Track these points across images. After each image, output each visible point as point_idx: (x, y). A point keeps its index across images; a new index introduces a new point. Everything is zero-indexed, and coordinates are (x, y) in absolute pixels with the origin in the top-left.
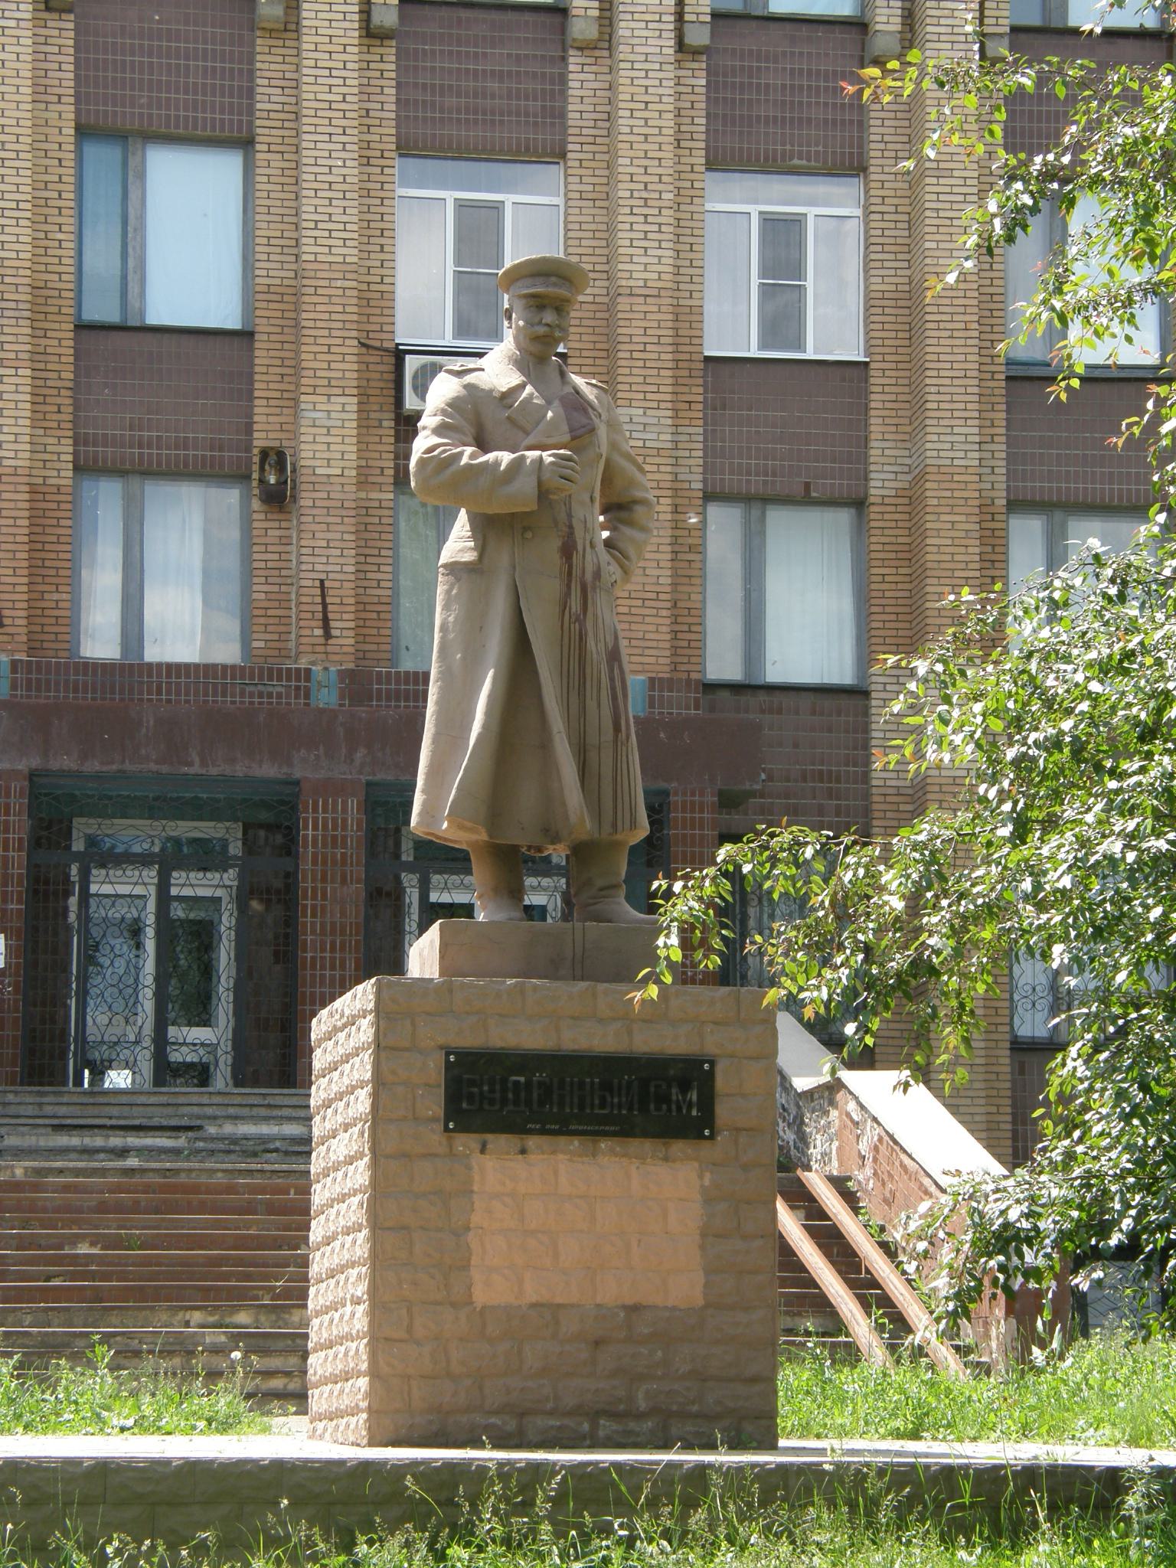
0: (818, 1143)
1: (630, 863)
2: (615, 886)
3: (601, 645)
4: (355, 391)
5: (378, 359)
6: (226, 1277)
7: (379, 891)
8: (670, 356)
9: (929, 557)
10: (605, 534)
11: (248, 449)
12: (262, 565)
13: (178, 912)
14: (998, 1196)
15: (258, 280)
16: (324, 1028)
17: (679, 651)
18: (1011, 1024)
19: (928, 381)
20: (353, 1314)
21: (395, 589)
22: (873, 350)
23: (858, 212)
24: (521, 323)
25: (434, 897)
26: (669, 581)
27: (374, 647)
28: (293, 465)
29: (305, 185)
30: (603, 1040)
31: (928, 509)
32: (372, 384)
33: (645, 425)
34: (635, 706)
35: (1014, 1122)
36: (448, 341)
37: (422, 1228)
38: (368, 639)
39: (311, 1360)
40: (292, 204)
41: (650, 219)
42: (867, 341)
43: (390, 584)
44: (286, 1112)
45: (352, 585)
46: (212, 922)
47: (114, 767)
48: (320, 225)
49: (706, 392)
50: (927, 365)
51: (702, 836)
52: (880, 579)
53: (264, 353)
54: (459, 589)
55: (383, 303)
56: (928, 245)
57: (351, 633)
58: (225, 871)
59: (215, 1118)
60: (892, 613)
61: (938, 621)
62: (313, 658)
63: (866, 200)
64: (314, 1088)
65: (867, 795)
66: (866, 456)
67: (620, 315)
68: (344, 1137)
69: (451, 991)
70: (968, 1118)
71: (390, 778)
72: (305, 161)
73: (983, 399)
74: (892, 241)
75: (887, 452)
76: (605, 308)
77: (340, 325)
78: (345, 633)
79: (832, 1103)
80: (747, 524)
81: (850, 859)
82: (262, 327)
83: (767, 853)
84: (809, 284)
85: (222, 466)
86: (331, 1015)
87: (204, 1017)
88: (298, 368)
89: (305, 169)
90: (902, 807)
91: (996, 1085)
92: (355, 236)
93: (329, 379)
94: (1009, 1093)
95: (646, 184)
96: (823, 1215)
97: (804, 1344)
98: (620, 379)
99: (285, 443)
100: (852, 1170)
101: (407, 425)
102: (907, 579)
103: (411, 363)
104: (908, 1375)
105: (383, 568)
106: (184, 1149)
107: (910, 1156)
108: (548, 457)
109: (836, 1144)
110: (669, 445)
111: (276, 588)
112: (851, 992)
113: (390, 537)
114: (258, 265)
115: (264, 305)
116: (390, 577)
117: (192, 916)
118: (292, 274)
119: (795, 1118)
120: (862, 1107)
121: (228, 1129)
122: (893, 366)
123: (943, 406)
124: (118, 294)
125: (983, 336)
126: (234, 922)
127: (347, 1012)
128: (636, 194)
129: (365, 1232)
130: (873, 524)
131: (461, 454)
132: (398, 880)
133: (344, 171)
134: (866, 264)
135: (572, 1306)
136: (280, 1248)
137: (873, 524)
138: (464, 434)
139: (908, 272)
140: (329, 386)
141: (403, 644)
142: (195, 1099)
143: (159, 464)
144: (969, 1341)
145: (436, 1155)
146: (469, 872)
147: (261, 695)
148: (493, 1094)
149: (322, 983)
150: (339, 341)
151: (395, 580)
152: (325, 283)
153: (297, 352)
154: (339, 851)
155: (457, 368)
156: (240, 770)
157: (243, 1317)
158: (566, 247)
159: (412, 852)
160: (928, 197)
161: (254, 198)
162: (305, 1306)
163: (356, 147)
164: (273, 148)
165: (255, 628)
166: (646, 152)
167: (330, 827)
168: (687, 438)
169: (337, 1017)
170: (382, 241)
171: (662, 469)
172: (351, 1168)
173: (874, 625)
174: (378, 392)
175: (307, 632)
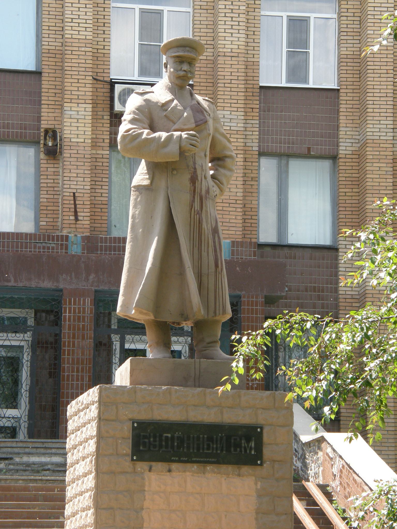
0: (313, 468)
2: (215, 342)
5: (102, 86)
7: (100, 343)
10: (212, 172)
11: (39, 129)
15: (44, 47)
16: (73, 410)
17: (246, 228)
22: (342, 83)
23: (335, 16)
24: (172, 70)
25: (127, 346)
26: (242, 194)
27: (99, 225)
28: (61, 137)
31: (368, 161)
32: (99, 98)
33: (231, 119)
34: (225, 255)
36: (136, 78)
38: (96, 221)
40: (61, 10)
41: (234, 19)
42: (338, 79)
43: (107, 195)
44: (53, 451)
45: (89, 195)
46: (19, 358)
48: (74, 21)
49: (260, 103)
50: (368, 91)
51: (257, 318)
54: (141, 197)
57: (88, 218)
58: (26, 333)
59: (19, 454)
60: (349, 210)
62: (69, 230)
63: (339, 10)
64: (68, 439)
65: (336, 299)
66: (338, 135)
67: (219, 66)
68: (82, 463)
69: (170, 393)
71: (106, 288)
74: (352, 30)
75: (348, 133)
78: (85, 218)
79: (320, 448)
82: (45, 70)
83: (288, 325)
84: (311, 51)
85: (25, 137)
86: (77, 403)
87: (14, 404)
88: (63, 90)
90: (354, 305)
92: (91, 26)
93: (78, 95)
96: (315, 503)
99: (56, 126)
100: (329, 482)
101: (116, 118)
102: (357, 194)
103: (118, 88)
106: (3, 469)
107: (358, 475)
108: (184, 135)
109: (321, 469)
111: (52, 197)
113: (107, 172)
116: (107, 191)
117: (9, 355)
119: (302, 455)
120: (334, 450)
121: (25, 459)
123: (375, 110)
126: (29, 358)
129: (92, 510)
130: (341, 168)
131: (142, 133)
132: (110, 338)
134: (338, 42)
136: (50, 518)
138: (144, 123)
140: (78, 99)
141: (113, 223)
142: (9, 445)
145: (127, 473)
147: (44, 248)
148: (155, 442)
149: (72, 388)
151: (110, 193)
153: (63, 82)
154: (81, 324)
155: (141, 91)
156: (33, 284)
158: (194, 32)
161: (42, 7)
165: (42, 216)
167: (77, 311)
168: (251, 125)
169: (80, 404)
170: (104, 28)
172: (86, 479)
173: (341, 216)
174: (102, 102)
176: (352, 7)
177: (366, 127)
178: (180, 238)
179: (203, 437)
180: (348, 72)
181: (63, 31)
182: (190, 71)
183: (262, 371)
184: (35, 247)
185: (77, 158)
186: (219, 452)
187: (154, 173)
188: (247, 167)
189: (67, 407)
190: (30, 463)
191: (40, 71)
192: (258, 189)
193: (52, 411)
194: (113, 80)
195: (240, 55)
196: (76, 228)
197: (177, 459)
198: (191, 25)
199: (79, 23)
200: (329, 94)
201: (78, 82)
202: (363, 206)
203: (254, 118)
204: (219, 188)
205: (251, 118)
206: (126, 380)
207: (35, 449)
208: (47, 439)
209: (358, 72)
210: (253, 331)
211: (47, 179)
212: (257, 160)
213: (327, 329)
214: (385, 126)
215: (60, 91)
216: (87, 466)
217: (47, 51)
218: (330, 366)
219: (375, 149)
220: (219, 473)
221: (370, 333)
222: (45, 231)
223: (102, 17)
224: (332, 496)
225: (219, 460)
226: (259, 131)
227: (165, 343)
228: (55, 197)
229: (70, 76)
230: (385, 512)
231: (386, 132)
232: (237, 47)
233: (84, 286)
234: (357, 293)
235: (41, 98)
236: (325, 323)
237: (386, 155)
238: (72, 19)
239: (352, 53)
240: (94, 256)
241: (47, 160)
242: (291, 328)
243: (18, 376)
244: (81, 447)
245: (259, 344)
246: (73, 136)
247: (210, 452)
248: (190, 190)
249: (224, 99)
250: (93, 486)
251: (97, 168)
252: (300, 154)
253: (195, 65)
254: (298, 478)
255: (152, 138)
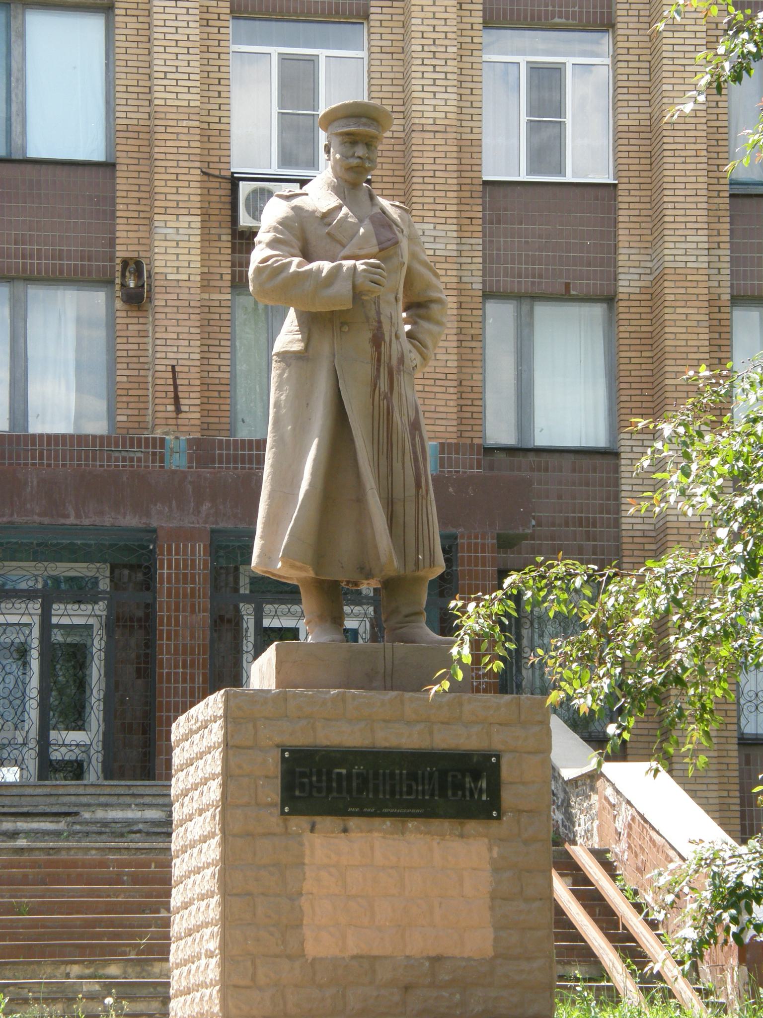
0: (582, 822)
1: (429, 594)
2: (418, 614)
3: (405, 418)
4: (199, 212)
5: (217, 185)
6: (99, 936)
7: (221, 618)
8: (455, 181)
9: (667, 343)
10: (407, 328)
11: (112, 259)
12: (125, 354)
13: (58, 637)
14: (733, 860)
15: (119, 121)
16: (182, 731)
17: (464, 421)
18: (738, 724)
19: (666, 199)
20: (207, 966)
21: (233, 373)
22: (620, 174)
23: (608, 61)
24: (338, 156)
25: (266, 623)
26: (455, 364)
27: (216, 420)
28: (149, 272)
29: (156, 43)
30: (409, 738)
31: (666, 304)
32: (213, 205)
33: (435, 237)
34: (431, 468)
35: (742, 804)
36: (274, 169)
37: (263, 894)
39: (173, 1004)
40: (147, 58)
41: (438, 69)
42: (615, 167)
43: (228, 369)
44: (147, 800)
45: (198, 369)
46: (85, 645)
47: (5, 519)
48: (169, 76)
49: (484, 209)
50: (665, 186)
52: (627, 361)
53: (124, 181)
54: (290, 372)
55: (222, 140)
56: (665, 87)
57: (198, 409)
58: (96, 603)
59: (89, 805)
60: (638, 388)
61: (675, 395)
62: (166, 429)
63: (614, 51)
64: (174, 780)
65: (618, 538)
66: (615, 261)
67: (414, 148)
68: (199, 820)
69: (344, 700)
70: (704, 801)
71: (230, 526)
72: (156, 23)
73: (711, 213)
74: (636, 84)
75: (632, 257)
76: (402, 142)
77: (186, 157)
78: (193, 409)
79: (593, 789)
80: (519, 316)
81: (612, 588)
82: (122, 160)
83: (544, 581)
84: (568, 120)
85: (90, 273)
86: (188, 720)
87: (80, 723)
88: (151, 194)
89: (156, 29)
90: (647, 547)
91: (727, 773)
92: (198, 84)
93: (178, 201)
94: (737, 780)
95: (434, 40)
96: (587, 881)
97: (574, 988)
98: (414, 200)
99: (142, 254)
100: (610, 844)
101: (244, 240)
102: (650, 361)
103: (245, 188)
104: (660, 1013)
105: (222, 356)
106: (64, 831)
107: (658, 833)
108: (360, 265)
109: (596, 823)
110: (455, 254)
111: (136, 373)
112: (611, 697)
113: (229, 330)
114: (118, 108)
115: (124, 141)
116: (228, 362)
117: (69, 640)
118: (146, 116)
119: (563, 801)
120: (618, 792)
121: (100, 814)
122: (637, 186)
123: (678, 219)
124: (4, 133)
125: (711, 162)
126: (103, 645)
127: (201, 718)
128: (426, 48)
129: (217, 898)
130: (621, 316)
131: (290, 263)
132: (237, 610)
133: (188, 31)
134: (614, 104)
135: (386, 957)
136: (143, 912)
137: (621, 316)
138: (293, 247)
139: (649, 110)
140: (177, 207)
141: (240, 417)
142: (72, 791)
143: (39, 272)
144: (709, 985)
145: (274, 834)
146: (298, 602)
147: (124, 459)
148: (321, 783)
149: (176, 695)
150: (186, 171)
151: (233, 365)
152: (174, 123)
153: (151, 180)
155: (286, 193)
156: (108, 521)
157: (113, 970)
158: (370, 92)
159: (248, 586)
160: (665, 48)
161: (114, 54)
162: (167, 960)
163: (197, 12)
164: (129, 12)
165: (119, 405)
166: (434, 13)
167: (182, 567)
169: (193, 721)
170: (220, 88)
171: (449, 272)
172: (205, 846)
173: (623, 398)
174: (217, 212)
175: (162, 408)
176: (636, 45)
177: (662, 247)
178: (356, 439)
179: (401, 774)
180: (631, 155)
181: (150, 93)
182: (368, 158)
183: (502, 659)
184: (109, 460)
185: (178, 307)
186: (427, 797)
187: (310, 330)
188: (464, 318)
189: (171, 726)
190: (108, 820)
191: (113, 161)
192: (483, 354)
193: (143, 734)
194: (236, 175)
195: (448, 129)
196: (177, 425)
197: (357, 810)
198: (366, 80)
199: (177, 80)
200: (601, 192)
201: (177, 180)
202: (660, 380)
203: (475, 235)
204: (421, 354)
205: (469, 234)
206: (269, 680)
207: (116, 798)
208: (136, 780)
209: (648, 155)
210: (484, 594)
211: (128, 343)
212: (480, 306)
213: (610, 587)
214: (694, 245)
215: (146, 195)
216: (206, 825)
217: (125, 128)
218: (614, 653)
219: (678, 284)
220: (428, 833)
221: (680, 595)
222: (125, 431)
223: (216, 69)
224: (616, 867)
225: (428, 811)
226: (484, 257)
227: (334, 618)
228: (142, 373)
229: (163, 170)
230: (708, 894)
231: (697, 256)
232: (443, 115)
233: (193, 523)
234: (652, 527)
235: (115, 207)
236: (604, 578)
237: (698, 295)
238: (166, 73)
239: (637, 123)
240: (208, 473)
241: (127, 311)
242: (550, 587)
243: (85, 676)
244: (196, 794)
245: (496, 614)
246: (169, 270)
247: (412, 797)
248: (372, 359)
249: (423, 204)
250: (218, 858)
251: (211, 323)
252: (552, 294)
253: (376, 148)
254: (561, 838)
255: (306, 271)
